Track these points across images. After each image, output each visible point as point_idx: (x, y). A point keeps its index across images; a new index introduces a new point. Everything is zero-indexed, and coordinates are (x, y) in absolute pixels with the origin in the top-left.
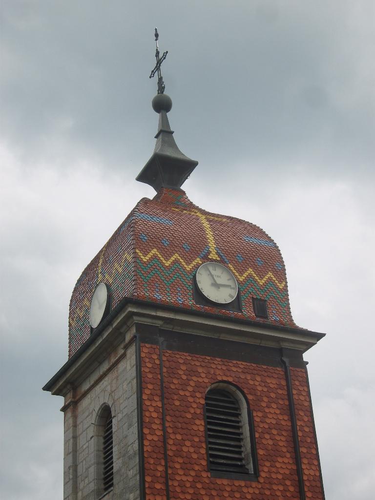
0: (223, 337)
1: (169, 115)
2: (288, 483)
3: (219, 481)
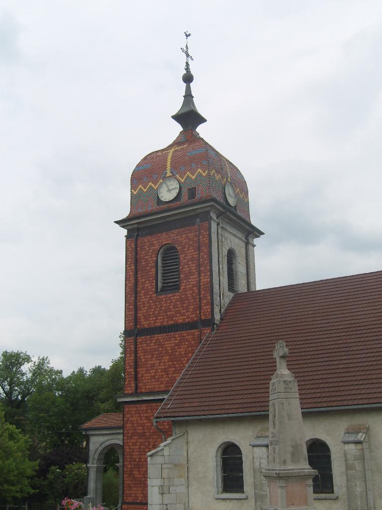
0: (168, 219)
1: (191, 84)
2: (195, 288)
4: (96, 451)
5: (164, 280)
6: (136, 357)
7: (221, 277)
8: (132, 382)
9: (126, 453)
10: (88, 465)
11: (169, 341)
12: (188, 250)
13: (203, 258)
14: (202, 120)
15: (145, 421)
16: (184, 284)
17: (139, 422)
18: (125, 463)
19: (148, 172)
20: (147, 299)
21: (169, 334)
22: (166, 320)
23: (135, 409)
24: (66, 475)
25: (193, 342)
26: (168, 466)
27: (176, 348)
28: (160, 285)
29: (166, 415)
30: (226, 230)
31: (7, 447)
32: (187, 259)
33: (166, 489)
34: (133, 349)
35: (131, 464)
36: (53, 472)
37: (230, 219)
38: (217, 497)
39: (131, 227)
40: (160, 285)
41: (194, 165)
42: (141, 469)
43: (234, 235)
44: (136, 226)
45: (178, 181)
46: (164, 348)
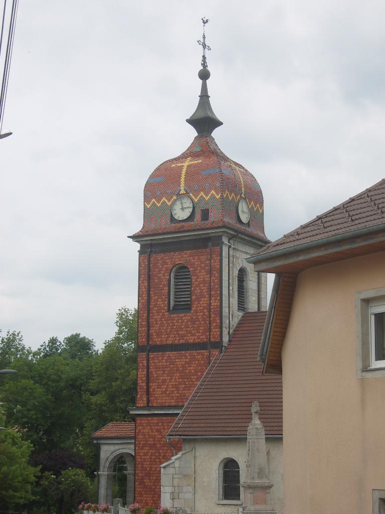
4: (107, 459)
5: (176, 298)
6: (148, 372)
7: (230, 298)
8: (144, 396)
9: (138, 463)
10: (99, 473)
11: (181, 359)
12: (200, 272)
13: (214, 282)
14: (218, 124)
15: (156, 433)
16: (195, 306)
17: (151, 434)
18: (137, 472)
19: (161, 183)
20: (159, 317)
21: (180, 352)
22: (177, 339)
23: (146, 422)
24: (62, 481)
25: (202, 362)
26: (179, 476)
27: (187, 366)
28: (172, 303)
29: (177, 433)
31: (10, 453)
32: (200, 277)
33: (176, 496)
34: (145, 365)
35: (142, 473)
36: (47, 478)
37: (242, 239)
38: (218, 502)
39: (145, 243)
40: (172, 303)
42: (151, 478)
44: (149, 242)
45: (192, 200)
46: (175, 366)
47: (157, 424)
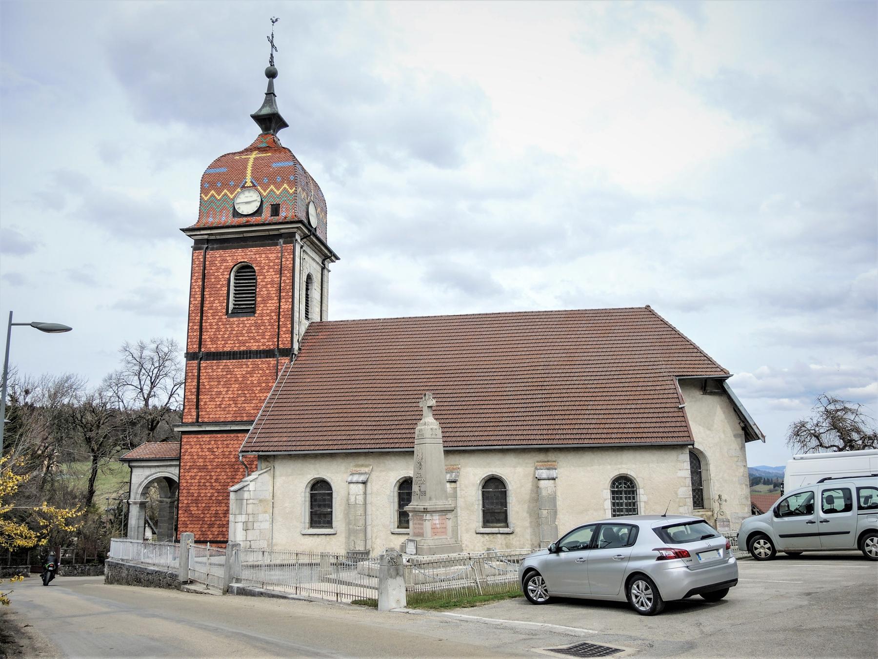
0: (246, 235)
3: (231, 320)
6: (198, 382)
11: (240, 368)
15: (207, 453)
23: (195, 440)
28: (231, 306)
29: (253, 449)
30: (307, 253)
32: (266, 280)
33: (250, 525)
37: (312, 243)
40: (231, 306)
41: (279, 179)
43: (313, 259)
44: (206, 237)
47: (209, 443)
